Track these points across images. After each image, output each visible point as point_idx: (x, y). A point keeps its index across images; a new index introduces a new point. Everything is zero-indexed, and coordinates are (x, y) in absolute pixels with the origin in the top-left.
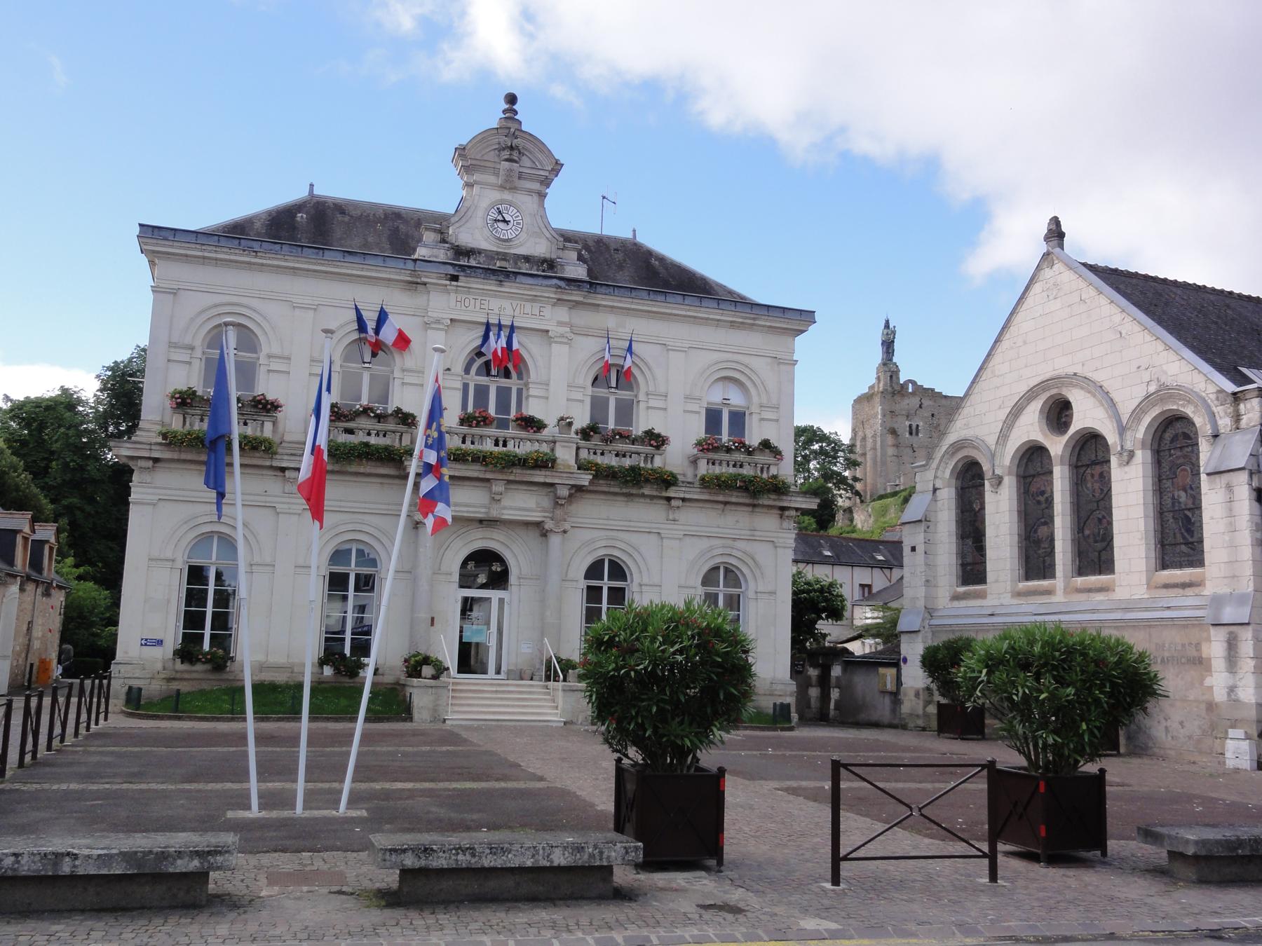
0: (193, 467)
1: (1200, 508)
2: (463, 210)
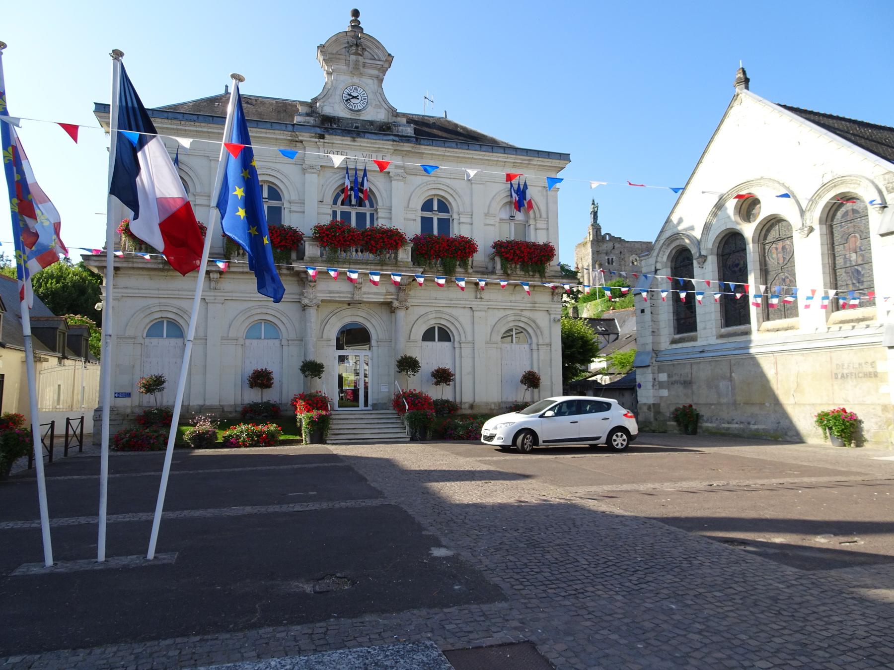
0: (145, 272)
1: (869, 262)
2: (326, 93)
